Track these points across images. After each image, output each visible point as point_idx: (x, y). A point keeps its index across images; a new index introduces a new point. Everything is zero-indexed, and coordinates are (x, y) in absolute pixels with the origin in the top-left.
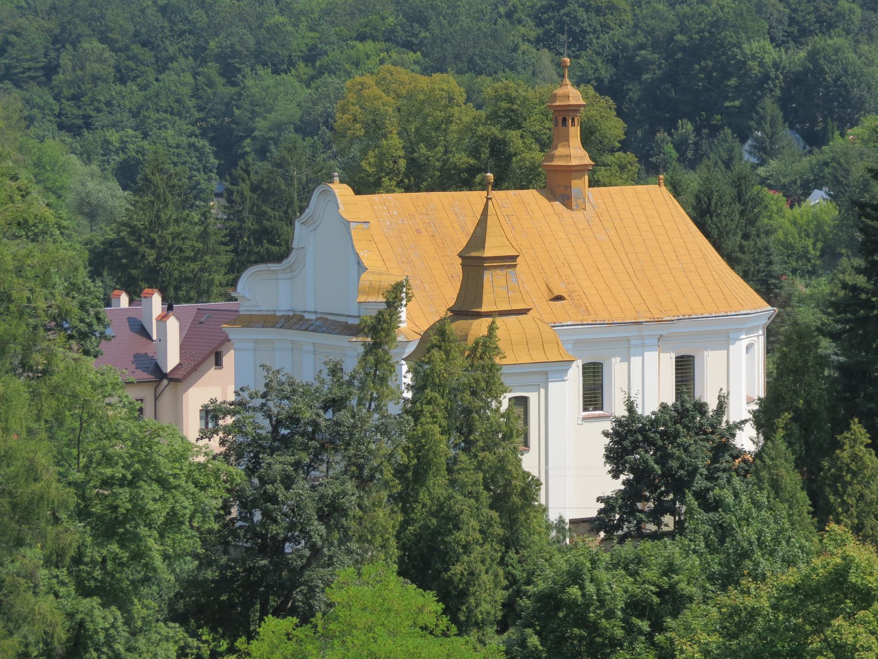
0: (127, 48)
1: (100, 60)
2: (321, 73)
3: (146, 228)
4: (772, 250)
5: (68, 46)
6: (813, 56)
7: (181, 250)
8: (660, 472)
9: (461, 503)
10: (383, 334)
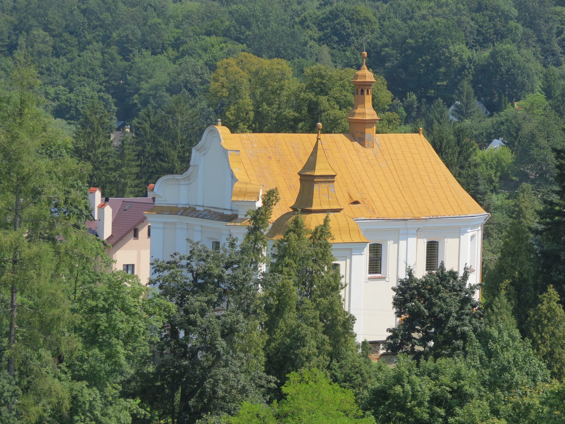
0: (60, 35)
1: (44, 42)
2: (182, 55)
3: (85, 149)
4: (479, 176)
5: (23, 32)
6: (493, 55)
7: (107, 163)
8: (428, 314)
9: (306, 330)
10: (260, 222)
